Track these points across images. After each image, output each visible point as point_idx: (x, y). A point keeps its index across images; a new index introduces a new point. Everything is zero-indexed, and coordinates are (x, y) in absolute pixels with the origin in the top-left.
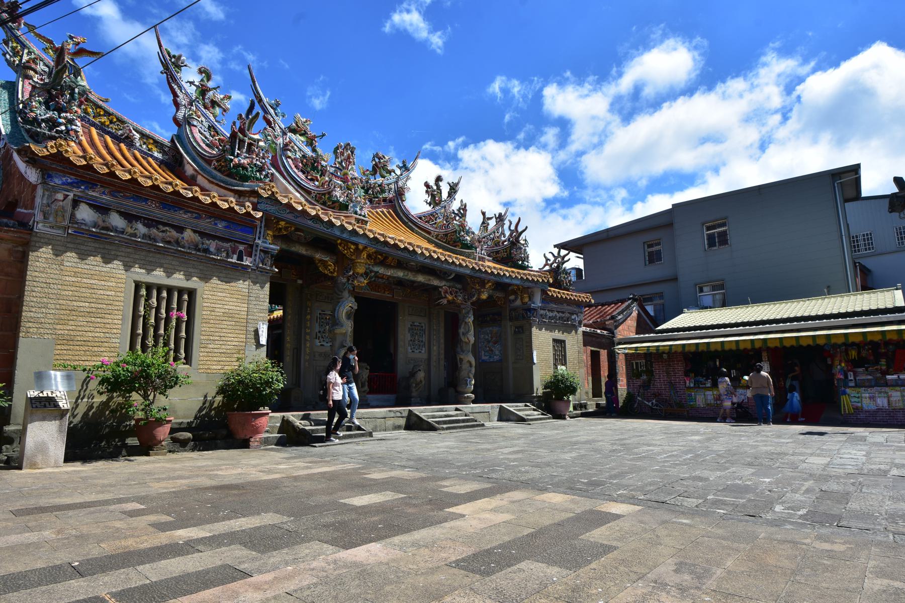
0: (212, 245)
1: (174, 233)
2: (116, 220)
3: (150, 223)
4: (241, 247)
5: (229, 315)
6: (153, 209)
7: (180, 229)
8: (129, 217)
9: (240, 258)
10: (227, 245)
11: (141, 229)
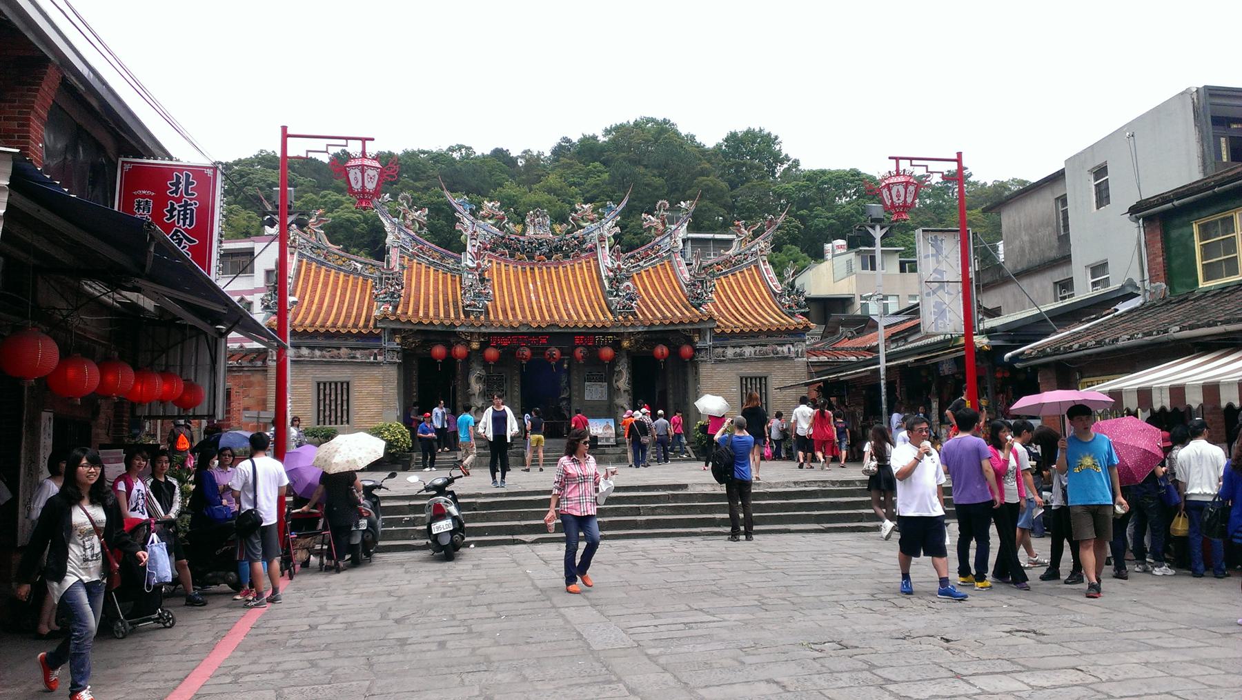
0: (358, 354)
1: (336, 352)
2: (305, 351)
3: (321, 348)
5: (370, 394)
6: (321, 341)
7: (339, 348)
8: (312, 348)
9: (375, 358)
11: (317, 353)
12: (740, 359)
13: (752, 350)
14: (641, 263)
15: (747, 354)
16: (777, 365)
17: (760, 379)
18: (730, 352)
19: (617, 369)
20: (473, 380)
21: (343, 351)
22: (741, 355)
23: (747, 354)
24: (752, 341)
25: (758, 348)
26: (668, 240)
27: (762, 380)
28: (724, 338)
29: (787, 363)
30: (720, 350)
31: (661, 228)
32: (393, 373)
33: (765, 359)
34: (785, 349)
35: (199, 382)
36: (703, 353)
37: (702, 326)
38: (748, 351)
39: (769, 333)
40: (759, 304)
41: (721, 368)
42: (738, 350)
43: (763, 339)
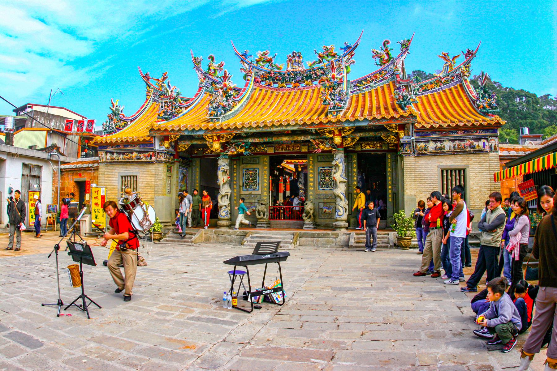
0: (142, 156)
1: (130, 155)
2: (115, 155)
3: (119, 153)
4: (151, 153)
6: (122, 148)
7: (132, 153)
9: (151, 159)
10: (147, 154)
11: (121, 156)
12: (440, 153)
13: (452, 144)
14: (372, 84)
15: (447, 149)
16: (474, 159)
17: (460, 171)
18: (431, 146)
19: (334, 163)
20: (220, 173)
21: (135, 154)
22: (441, 148)
23: (447, 149)
24: (452, 136)
25: (457, 143)
26: (391, 66)
27: (462, 172)
28: (425, 133)
29: (483, 157)
30: (423, 144)
31: (386, 58)
32: (162, 168)
33: (464, 152)
34: (481, 143)
35: (485, 279)
36: (407, 147)
37: (404, 122)
38: (448, 145)
39: (466, 129)
40: (462, 110)
41: (423, 161)
42: (439, 145)
43: (460, 134)
